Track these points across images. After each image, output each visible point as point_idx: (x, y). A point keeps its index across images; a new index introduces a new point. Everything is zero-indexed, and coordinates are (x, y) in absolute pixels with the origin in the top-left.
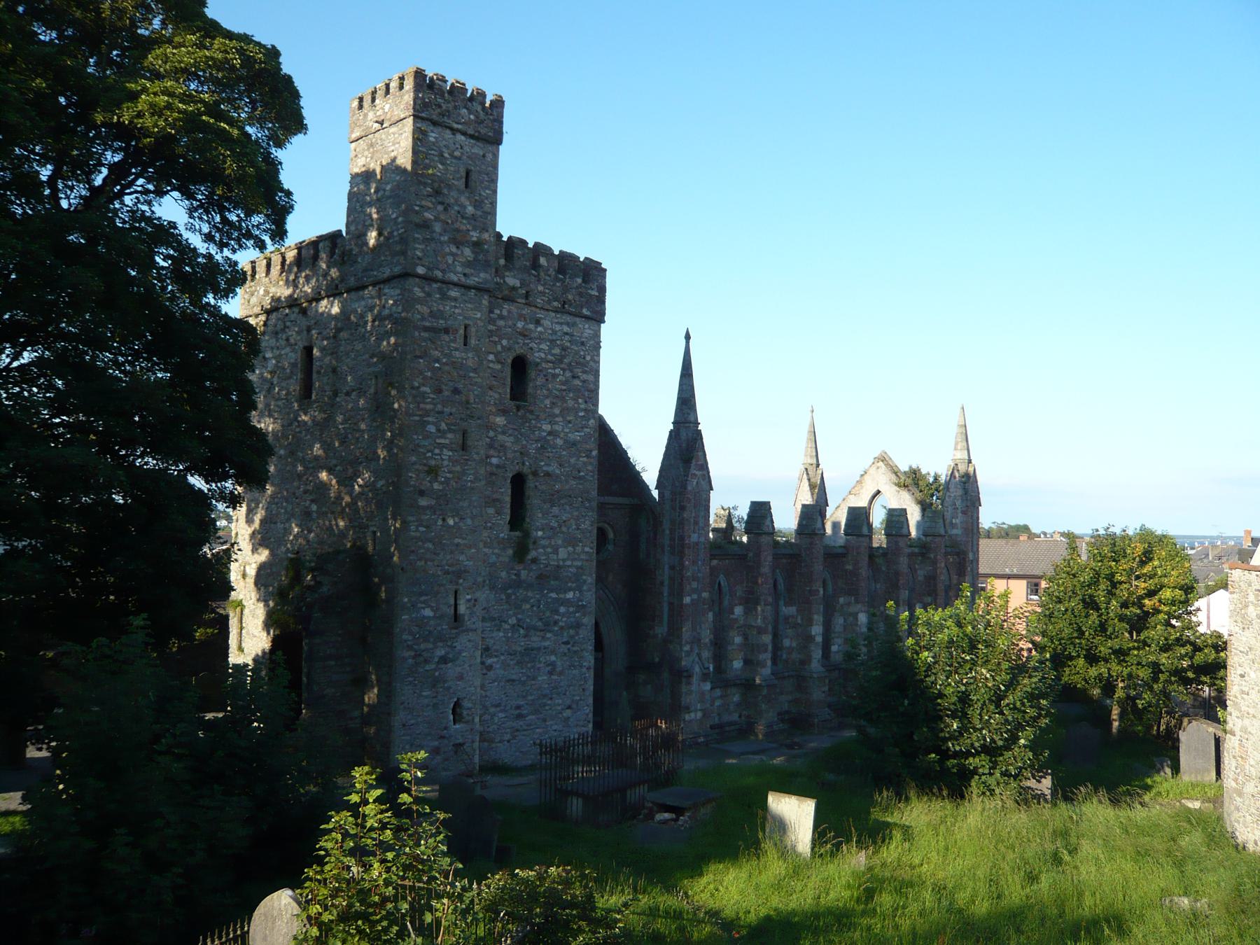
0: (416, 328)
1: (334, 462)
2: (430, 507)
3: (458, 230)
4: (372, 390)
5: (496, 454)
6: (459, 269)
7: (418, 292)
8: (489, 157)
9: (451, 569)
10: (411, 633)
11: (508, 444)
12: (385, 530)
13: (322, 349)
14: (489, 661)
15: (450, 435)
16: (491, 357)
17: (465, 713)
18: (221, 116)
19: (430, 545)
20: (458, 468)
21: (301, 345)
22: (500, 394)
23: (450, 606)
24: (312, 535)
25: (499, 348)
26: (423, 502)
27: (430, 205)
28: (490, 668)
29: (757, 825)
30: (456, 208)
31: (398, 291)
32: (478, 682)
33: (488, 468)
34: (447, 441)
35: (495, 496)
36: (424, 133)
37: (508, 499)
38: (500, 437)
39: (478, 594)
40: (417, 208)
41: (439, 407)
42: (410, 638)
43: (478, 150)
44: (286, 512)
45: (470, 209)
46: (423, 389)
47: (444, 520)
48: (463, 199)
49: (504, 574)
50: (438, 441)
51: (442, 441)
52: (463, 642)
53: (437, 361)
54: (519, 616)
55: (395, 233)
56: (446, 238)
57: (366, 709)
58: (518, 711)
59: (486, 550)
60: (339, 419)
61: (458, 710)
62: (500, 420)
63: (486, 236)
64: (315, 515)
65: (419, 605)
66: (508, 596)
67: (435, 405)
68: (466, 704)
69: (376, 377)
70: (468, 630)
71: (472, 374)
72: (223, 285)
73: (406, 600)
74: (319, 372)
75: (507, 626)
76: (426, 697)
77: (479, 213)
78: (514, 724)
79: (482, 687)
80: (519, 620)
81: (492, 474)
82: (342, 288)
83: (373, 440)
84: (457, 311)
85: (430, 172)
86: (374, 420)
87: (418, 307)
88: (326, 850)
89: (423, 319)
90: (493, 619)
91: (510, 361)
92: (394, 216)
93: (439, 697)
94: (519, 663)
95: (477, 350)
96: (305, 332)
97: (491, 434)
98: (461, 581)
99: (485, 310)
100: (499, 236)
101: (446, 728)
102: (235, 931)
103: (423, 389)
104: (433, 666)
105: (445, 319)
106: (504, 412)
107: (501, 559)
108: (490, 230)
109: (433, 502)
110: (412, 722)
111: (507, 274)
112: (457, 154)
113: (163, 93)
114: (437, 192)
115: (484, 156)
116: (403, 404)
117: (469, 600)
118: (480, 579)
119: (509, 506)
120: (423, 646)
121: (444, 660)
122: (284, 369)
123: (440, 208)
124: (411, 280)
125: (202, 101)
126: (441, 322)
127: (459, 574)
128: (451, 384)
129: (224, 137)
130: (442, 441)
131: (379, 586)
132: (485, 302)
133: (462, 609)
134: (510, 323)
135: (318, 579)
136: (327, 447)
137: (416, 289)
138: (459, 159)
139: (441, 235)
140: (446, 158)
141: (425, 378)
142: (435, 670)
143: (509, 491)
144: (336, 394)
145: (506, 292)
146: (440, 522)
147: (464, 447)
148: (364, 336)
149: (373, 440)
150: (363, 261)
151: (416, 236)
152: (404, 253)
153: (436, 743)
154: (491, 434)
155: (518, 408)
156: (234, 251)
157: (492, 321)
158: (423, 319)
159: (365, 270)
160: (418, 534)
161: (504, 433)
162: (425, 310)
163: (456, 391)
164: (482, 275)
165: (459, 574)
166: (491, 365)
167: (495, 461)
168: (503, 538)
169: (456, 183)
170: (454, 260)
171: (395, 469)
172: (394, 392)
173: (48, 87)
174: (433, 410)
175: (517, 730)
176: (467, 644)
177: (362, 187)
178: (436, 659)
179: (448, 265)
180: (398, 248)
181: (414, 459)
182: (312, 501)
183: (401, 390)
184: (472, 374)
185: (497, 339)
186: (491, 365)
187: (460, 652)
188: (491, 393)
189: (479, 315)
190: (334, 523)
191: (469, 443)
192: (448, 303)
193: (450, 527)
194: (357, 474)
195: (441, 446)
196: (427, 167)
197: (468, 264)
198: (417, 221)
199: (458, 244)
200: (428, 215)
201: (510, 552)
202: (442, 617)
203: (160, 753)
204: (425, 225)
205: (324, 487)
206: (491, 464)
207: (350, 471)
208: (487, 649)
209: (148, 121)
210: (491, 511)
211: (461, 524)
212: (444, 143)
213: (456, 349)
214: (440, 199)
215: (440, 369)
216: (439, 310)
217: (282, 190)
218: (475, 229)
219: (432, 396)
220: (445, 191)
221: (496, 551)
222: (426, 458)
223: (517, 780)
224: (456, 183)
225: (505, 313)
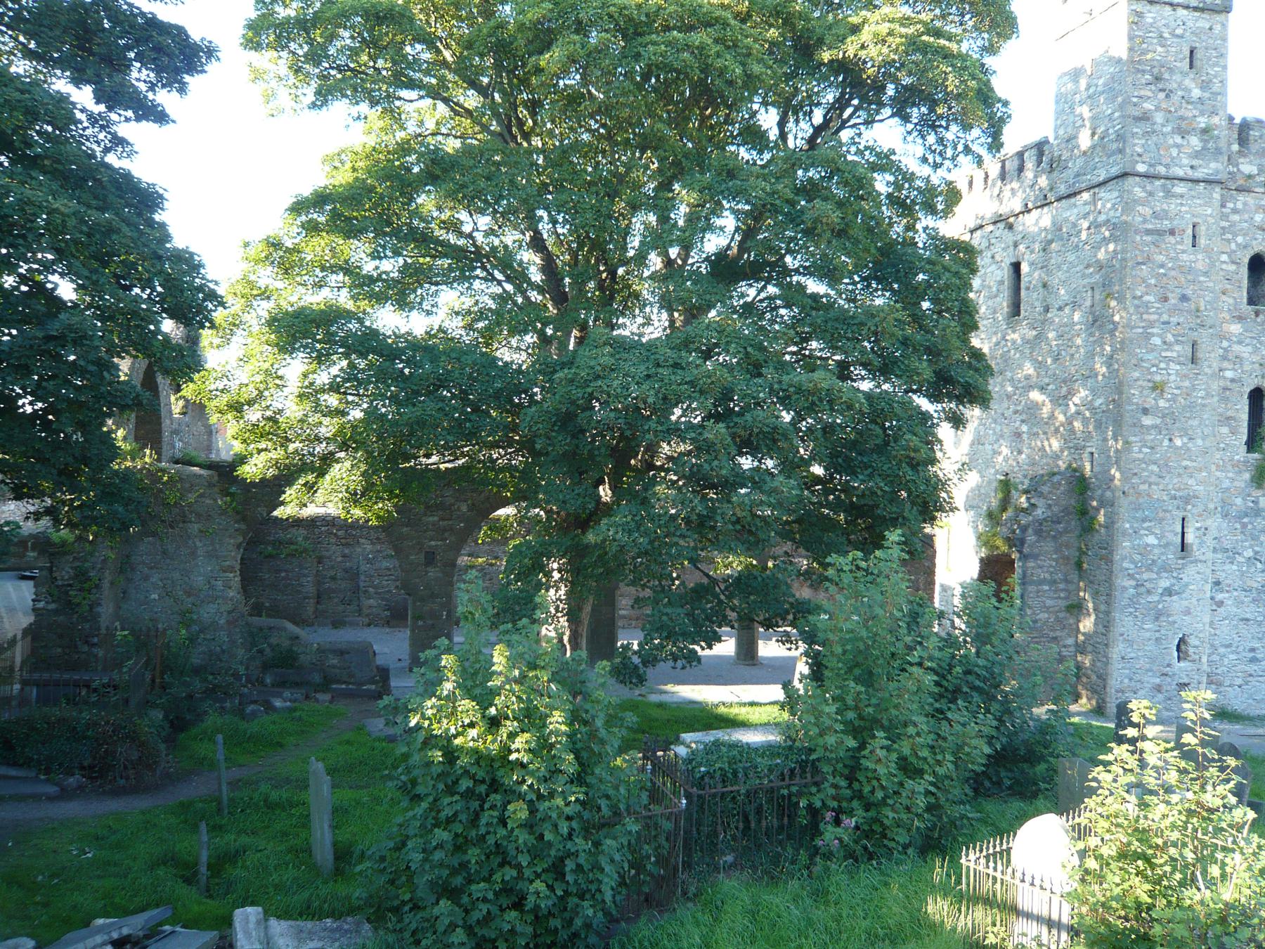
0: (1136, 232)
1: (1047, 380)
2: (1155, 427)
3: (1182, 118)
4: (1088, 303)
5: (1231, 367)
6: (1185, 161)
7: (1139, 192)
8: (1217, 28)
9: (1178, 494)
10: (1133, 562)
11: (1246, 355)
12: (1104, 451)
13: (1031, 264)
14: (1220, 597)
15: (1177, 348)
16: (1224, 257)
17: (1191, 650)
18: (938, 33)
19: (1155, 468)
20: (1187, 384)
21: (1008, 261)
22: (1235, 298)
23: (1176, 534)
24: (1023, 456)
25: (1233, 246)
26: (1147, 421)
27: (1150, 94)
28: (1220, 604)
29: (717, 744)
30: (1180, 93)
31: (1116, 194)
32: (1207, 619)
33: (1222, 383)
34: (1175, 354)
35: (1229, 413)
36: (1139, 14)
37: (1244, 416)
38: (1236, 348)
39: (1209, 522)
40: (1135, 100)
41: (1165, 317)
42: (1132, 566)
43: (1203, 21)
44: (995, 433)
45: (1196, 93)
46: (1147, 298)
47: (1170, 440)
48: (1187, 82)
49: (1239, 501)
50: (1164, 354)
51: (1169, 354)
52: (1190, 573)
53: (1162, 266)
54: (1257, 549)
55: (1111, 131)
56: (1169, 128)
57: (1081, 638)
58: (1251, 655)
59: (1218, 474)
60: (1051, 335)
61: (1183, 647)
62: (1236, 328)
63: (1216, 120)
64: (1025, 436)
65: (1142, 532)
66: (1244, 526)
67: (1160, 315)
68: (1193, 641)
69: (1093, 289)
70: (1196, 561)
71: (1202, 279)
72: (940, 207)
73: (1127, 526)
74: (1028, 289)
75: (1241, 559)
76: (1148, 630)
77: (1207, 95)
78: (1247, 668)
79: (1211, 623)
80: (1256, 553)
81: (1225, 389)
82: (1051, 198)
83: (1091, 355)
84: (1183, 209)
85: (1149, 57)
86: (1091, 335)
87: (1140, 208)
88: (1099, 782)
89: (1145, 221)
90: (1227, 550)
91: (1246, 260)
92: (1109, 111)
93: (1163, 632)
94: (1254, 600)
95: (1207, 251)
96: (1012, 248)
97: (1225, 344)
98: (1189, 507)
99: (1217, 204)
100: (1231, 119)
101: (1169, 665)
102: (995, 847)
103: (1147, 298)
104: (1156, 598)
105: (1171, 219)
106: (1240, 318)
107: (1237, 484)
108: (1221, 113)
109: (1158, 421)
110: (1133, 655)
111: (1241, 160)
112: (1179, 31)
113: (883, 20)
114: (1158, 79)
115: (1211, 29)
116: (1124, 314)
117: (1198, 529)
118: (1212, 506)
119: (1246, 424)
120: (1145, 576)
121: (1169, 592)
122: (990, 287)
123: (1162, 95)
124: (1131, 180)
125: (920, 22)
126: (1166, 222)
127: (1187, 500)
128: (1179, 290)
129: (947, 55)
130: (1169, 354)
131: (1097, 510)
132: (1217, 196)
133: (1190, 538)
134: (1246, 216)
135: (1033, 501)
136: (1040, 365)
137: (1137, 189)
138: (1181, 37)
139: (1163, 126)
140: (1166, 39)
141: (1148, 286)
142: (1159, 602)
143: (1247, 408)
144: (1047, 310)
145: (1241, 182)
146: (1166, 443)
147: (1194, 360)
148: (1077, 246)
149: (1091, 355)
150: (1075, 166)
151: (1135, 130)
152: (1121, 151)
153: (1158, 681)
154: (1225, 344)
155: (1257, 314)
156: (949, 170)
157: (1224, 217)
158: (1145, 221)
159: (1077, 175)
160: (1141, 456)
161: (1240, 342)
162: (1147, 211)
163: (1184, 298)
164: (1213, 165)
165: (1187, 500)
166: (1224, 266)
167: (1229, 374)
168: (1239, 461)
169: (1178, 64)
170: (1180, 152)
171: (1117, 387)
172: (1113, 303)
173: (781, 35)
174: (1158, 320)
175: (1251, 675)
176: (1195, 577)
177: (1069, 86)
178: (1160, 591)
179: (1173, 158)
180: (1115, 146)
181: (1137, 374)
182: (1023, 421)
183: (1121, 300)
184: (1202, 279)
185: (1230, 236)
186: (1224, 266)
187: (1187, 585)
188: (1224, 298)
189: (1209, 211)
190: (1046, 443)
191: (1200, 355)
192: (1173, 200)
193: (1178, 448)
194: (1071, 393)
195: (1169, 360)
196: (1144, 53)
197: (1197, 155)
198: (1137, 114)
199: (1183, 133)
200: (1148, 106)
201: (1247, 476)
202: (1167, 545)
203: (911, 664)
204: (1145, 118)
205: (1036, 406)
206: (1225, 378)
207: (1065, 389)
208: (1217, 583)
209: (873, 51)
210: (1225, 430)
211: (1190, 445)
212: (1163, 22)
213: (1184, 252)
214: (1160, 86)
215: (1165, 275)
216: (1163, 210)
217: (999, 100)
218: (1202, 114)
219: (1156, 305)
220: (1166, 76)
221: (1230, 475)
222: (1150, 373)
223: (1252, 731)
224: (1178, 64)
225: (1240, 205)
